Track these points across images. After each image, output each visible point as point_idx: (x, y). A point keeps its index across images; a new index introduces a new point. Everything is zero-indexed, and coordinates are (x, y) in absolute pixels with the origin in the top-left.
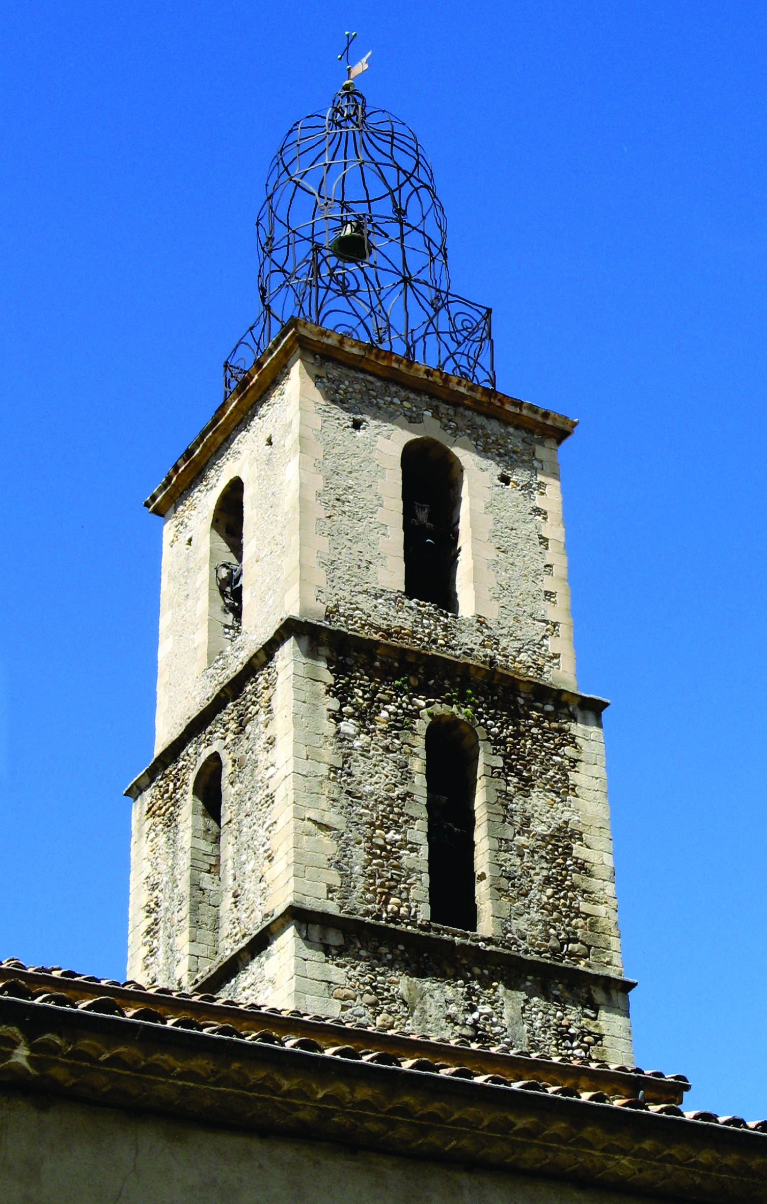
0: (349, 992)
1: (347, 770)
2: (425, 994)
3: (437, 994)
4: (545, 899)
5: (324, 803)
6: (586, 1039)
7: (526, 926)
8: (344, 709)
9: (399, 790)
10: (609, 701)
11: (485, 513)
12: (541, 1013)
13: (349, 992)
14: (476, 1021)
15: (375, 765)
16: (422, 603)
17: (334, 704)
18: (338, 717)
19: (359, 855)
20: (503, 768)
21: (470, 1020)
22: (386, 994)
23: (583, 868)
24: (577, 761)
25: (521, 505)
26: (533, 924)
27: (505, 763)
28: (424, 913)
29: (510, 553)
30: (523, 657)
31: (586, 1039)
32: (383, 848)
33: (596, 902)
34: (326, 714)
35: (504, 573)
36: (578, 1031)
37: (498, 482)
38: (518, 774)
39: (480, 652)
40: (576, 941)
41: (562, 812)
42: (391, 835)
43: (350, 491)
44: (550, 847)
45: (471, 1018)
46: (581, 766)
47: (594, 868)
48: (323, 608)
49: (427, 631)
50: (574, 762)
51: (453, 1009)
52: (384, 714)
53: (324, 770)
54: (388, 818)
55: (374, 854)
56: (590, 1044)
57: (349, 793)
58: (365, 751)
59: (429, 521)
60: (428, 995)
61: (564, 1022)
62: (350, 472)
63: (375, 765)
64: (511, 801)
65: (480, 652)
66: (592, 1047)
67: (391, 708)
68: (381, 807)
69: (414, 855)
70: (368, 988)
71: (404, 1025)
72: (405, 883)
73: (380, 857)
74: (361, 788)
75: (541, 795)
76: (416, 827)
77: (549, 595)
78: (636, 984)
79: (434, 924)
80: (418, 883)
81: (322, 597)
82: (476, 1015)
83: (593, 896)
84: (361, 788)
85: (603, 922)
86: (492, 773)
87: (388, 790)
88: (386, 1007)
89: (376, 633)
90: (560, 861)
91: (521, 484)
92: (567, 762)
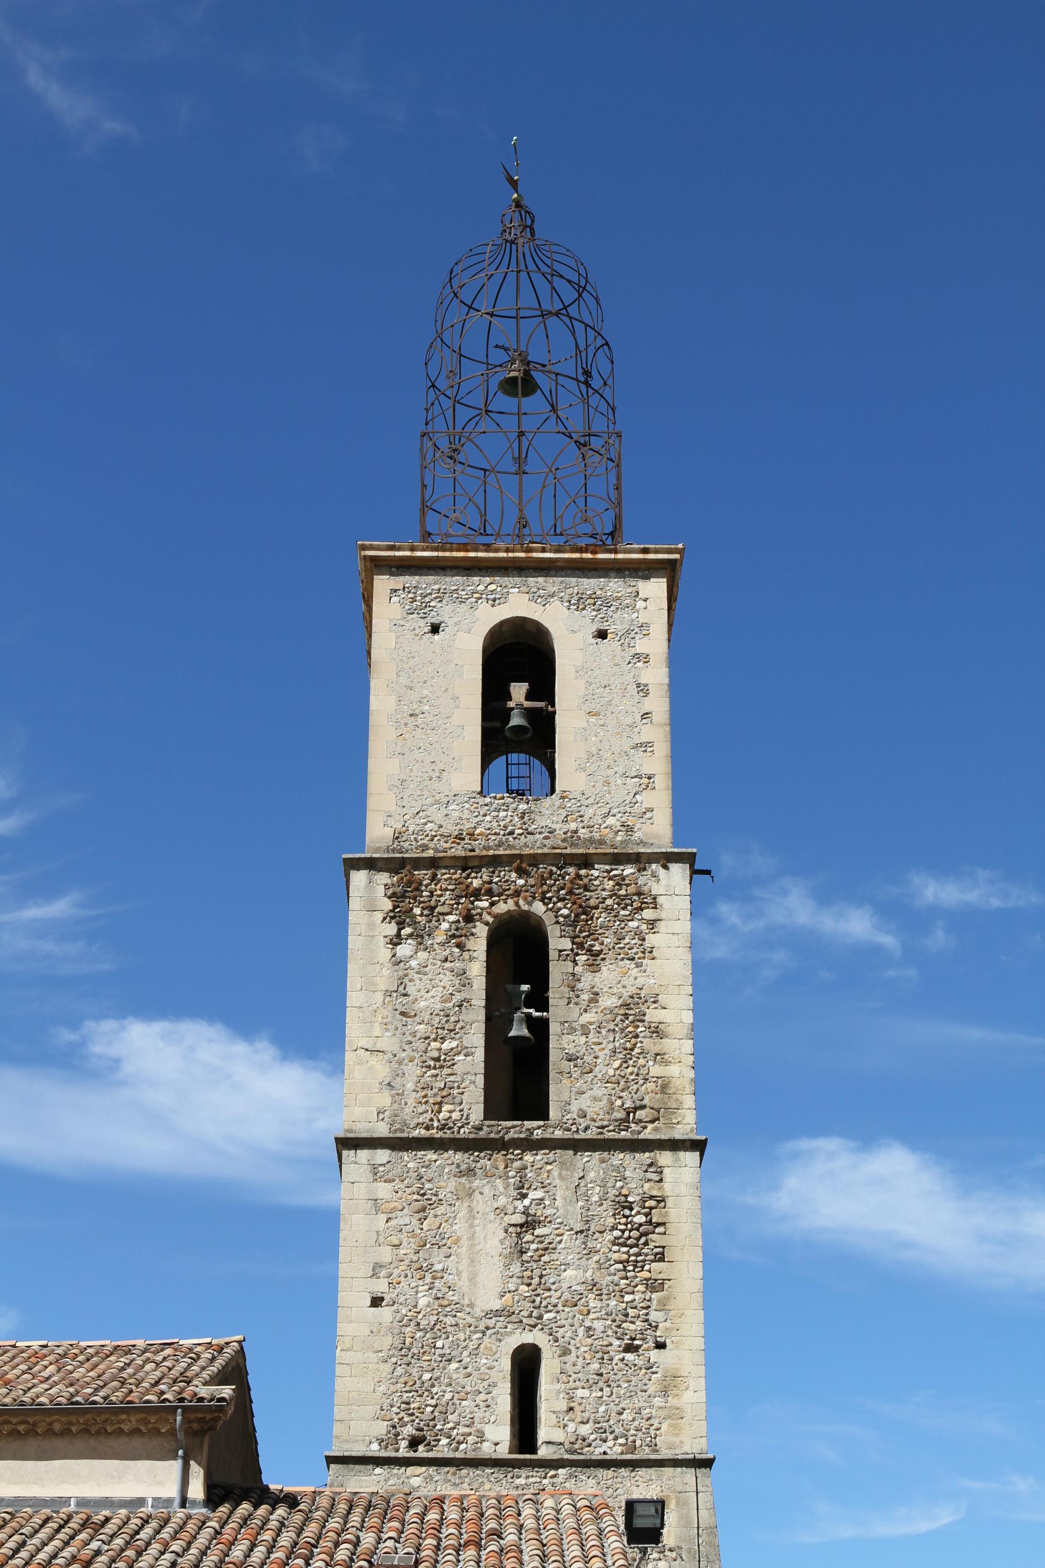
0: (395, 1204)
1: (403, 991)
2: (474, 1191)
3: (486, 1190)
4: (611, 1072)
5: (377, 1030)
6: (647, 1204)
7: (588, 1104)
8: (403, 932)
9: (458, 997)
10: (695, 850)
11: (576, 678)
12: (598, 1188)
13: (395, 1204)
14: (527, 1208)
15: (431, 980)
16: (499, 796)
17: (391, 929)
18: (396, 941)
19: (413, 1071)
20: (572, 950)
21: (521, 1208)
22: (434, 1198)
23: (657, 1031)
24: (655, 921)
25: (618, 657)
26: (595, 1099)
27: (573, 943)
28: (477, 1114)
29: (603, 713)
30: (611, 821)
31: (647, 1204)
32: (438, 1059)
33: (667, 1063)
34: (382, 941)
35: (593, 739)
36: (638, 1198)
37: (594, 641)
38: (589, 950)
39: (560, 829)
40: (643, 1107)
41: (636, 978)
42: (446, 1046)
43: (424, 701)
44: (619, 1018)
45: (520, 1206)
46: (661, 926)
47: (669, 1029)
48: (390, 832)
49: (502, 823)
50: (652, 924)
51: (502, 1201)
52: (445, 926)
53: (379, 997)
54: (443, 1028)
55: (429, 1067)
56: (651, 1208)
57: (403, 1014)
58: (422, 970)
59: (526, 699)
60: (477, 1192)
61: (624, 1192)
62: (425, 682)
63: (431, 980)
64: (579, 980)
65: (560, 829)
66: (653, 1211)
67: (452, 918)
68: (437, 1019)
69: (469, 1058)
70: (415, 1197)
71: (452, 1225)
72: (459, 1088)
73: (435, 1068)
74: (416, 1006)
75: (613, 967)
76: (472, 1031)
77: (645, 746)
78: (706, 1140)
79: (487, 1123)
80: (472, 1086)
81: (391, 821)
82: (527, 1202)
83: (666, 1057)
84: (416, 1006)
85: (676, 1083)
86: (560, 956)
87: (445, 1001)
88: (432, 1212)
89: (446, 842)
90: (630, 1029)
91: (620, 634)
92: (644, 927)
